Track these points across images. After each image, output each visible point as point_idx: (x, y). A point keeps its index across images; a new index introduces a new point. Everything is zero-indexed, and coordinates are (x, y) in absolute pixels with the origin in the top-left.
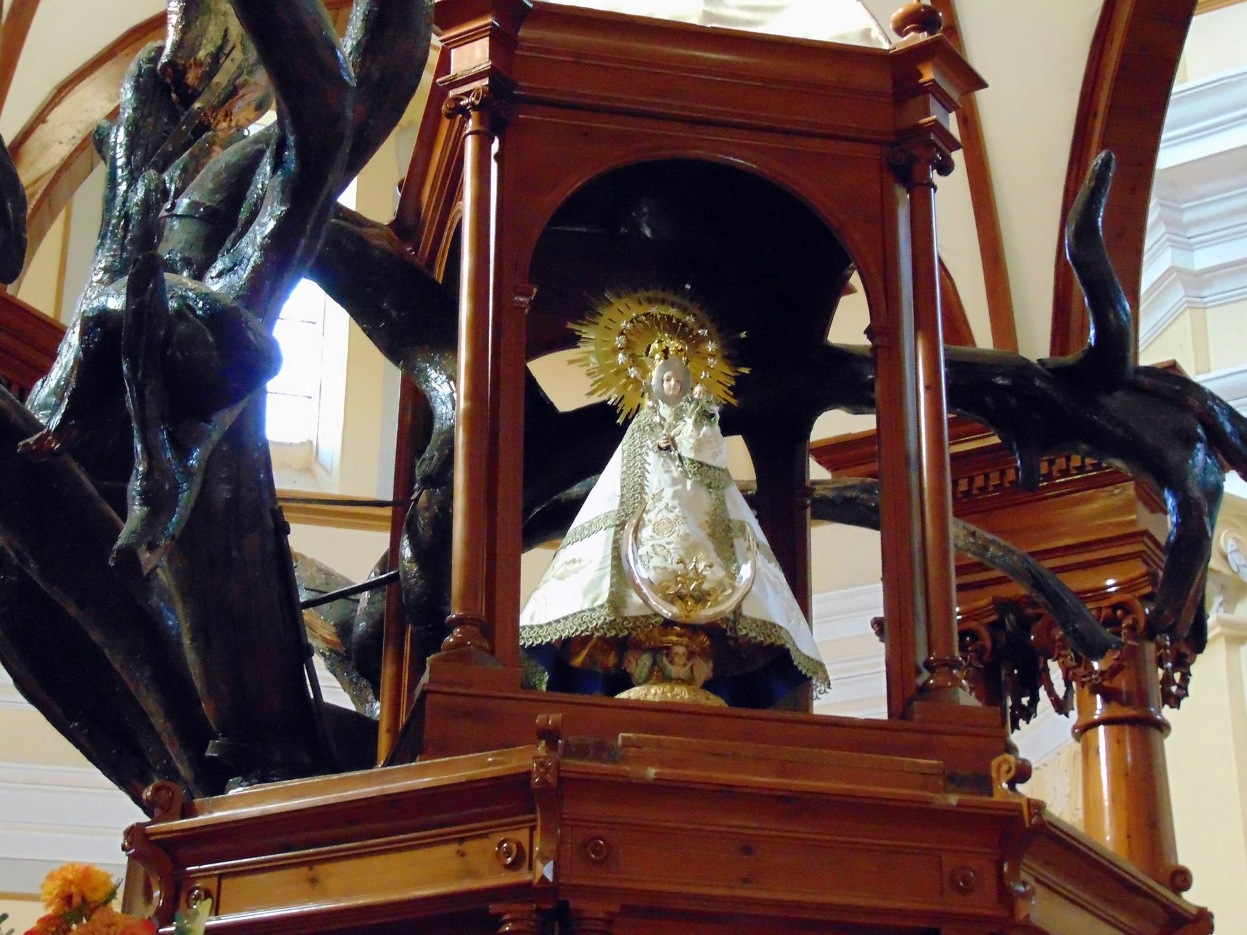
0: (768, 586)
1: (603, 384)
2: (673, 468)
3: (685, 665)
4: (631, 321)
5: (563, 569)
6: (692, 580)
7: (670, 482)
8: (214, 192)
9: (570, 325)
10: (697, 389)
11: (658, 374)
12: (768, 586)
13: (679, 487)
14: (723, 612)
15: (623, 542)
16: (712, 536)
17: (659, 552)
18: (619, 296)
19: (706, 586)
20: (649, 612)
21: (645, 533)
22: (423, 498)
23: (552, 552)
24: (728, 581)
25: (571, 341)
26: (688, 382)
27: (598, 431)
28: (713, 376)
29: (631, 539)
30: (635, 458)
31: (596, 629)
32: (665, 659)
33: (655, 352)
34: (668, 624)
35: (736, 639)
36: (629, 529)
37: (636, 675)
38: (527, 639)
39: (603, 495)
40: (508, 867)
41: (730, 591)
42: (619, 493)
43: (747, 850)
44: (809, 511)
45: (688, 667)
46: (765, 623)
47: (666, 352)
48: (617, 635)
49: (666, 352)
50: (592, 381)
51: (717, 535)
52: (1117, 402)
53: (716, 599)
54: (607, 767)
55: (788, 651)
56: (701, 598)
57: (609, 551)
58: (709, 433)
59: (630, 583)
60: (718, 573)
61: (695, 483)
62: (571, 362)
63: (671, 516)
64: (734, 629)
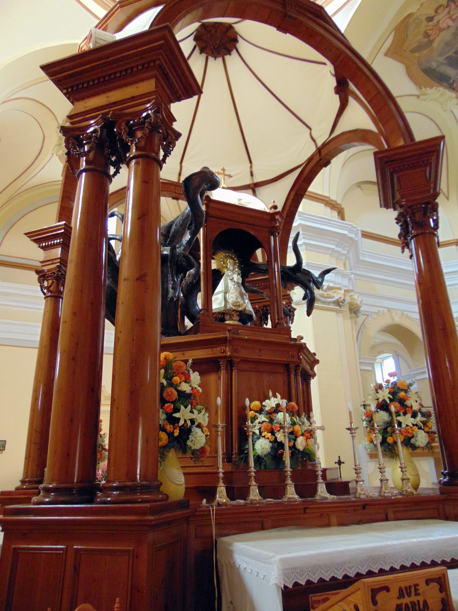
8: (165, 231)
17: (232, 297)
34: (234, 310)
38: (213, 312)
40: (222, 353)
43: (260, 351)
52: (298, 274)
54: (238, 336)
56: (239, 306)
60: (242, 302)
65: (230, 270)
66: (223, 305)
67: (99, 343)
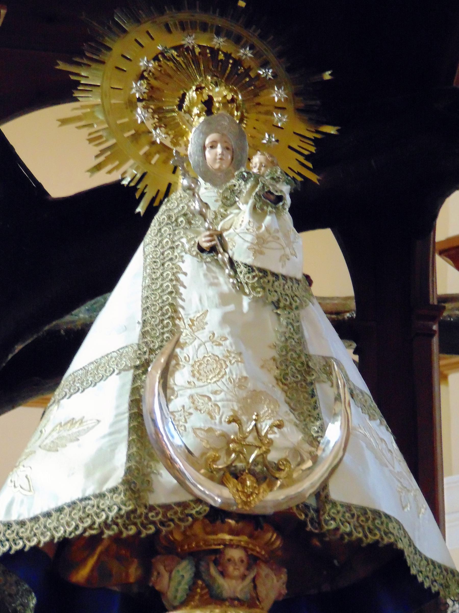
0: (368, 455)
1: (113, 154)
2: (221, 280)
3: (244, 577)
4: (156, 59)
5: (55, 435)
6: (251, 447)
7: (217, 300)
9: (62, 66)
10: (257, 159)
11: (198, 139)
12: (368, 455)
13: (231, 307)
14: (300, 495)
15: (146, 394)
16: (282, 380)
18: (138, 21)
19: (273, 457)
20: (185, 497)
21: (180, 378)
23: (41, 410)
24: (307, 447)
25: (62, 91)
26: (243, 149)
27: (110, 225)
28: (282, 139)
29: (157, 387)
31: (107, 525)
32: (213, 571)
33: (192, 104)
34: (216, 515)
35: (321, 536)
36: (155, 373)
37: (170, 594)
39: (115, 323)
41: (309, 464)
42: (139, 317)
44: (435, 340)
45: (248, 580)
46: (364, 511)
47: (208, 104)
48: (139, 533)
49: (208, 104)
50: (97, 150)
51: (290, 379)
53: (289, 476)
55: (401, 553)
56: (267, 474)
57: (125, 406)
58: (276, 226)
59: (157, 453)
61: (255, 300)
62: (64, 122)
63: (218, 351)
64: (317, 522)
65: (188, 203)
66: (117, 477)
67: (438, 344)
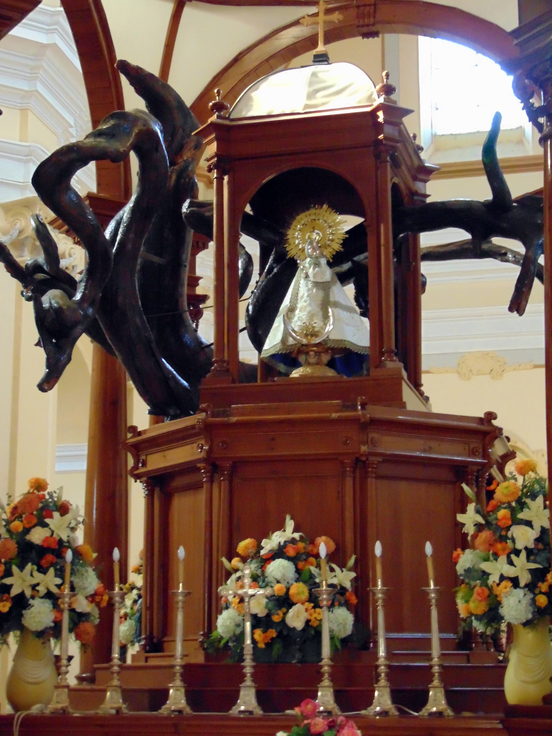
13: (310, 292)
19: (316, 329)
22: (138, 320)
25: (347, 232)
30: (298, 283)
56: (314, 334)
